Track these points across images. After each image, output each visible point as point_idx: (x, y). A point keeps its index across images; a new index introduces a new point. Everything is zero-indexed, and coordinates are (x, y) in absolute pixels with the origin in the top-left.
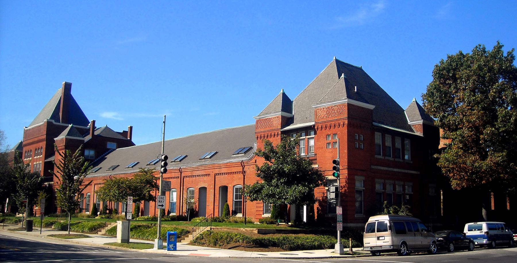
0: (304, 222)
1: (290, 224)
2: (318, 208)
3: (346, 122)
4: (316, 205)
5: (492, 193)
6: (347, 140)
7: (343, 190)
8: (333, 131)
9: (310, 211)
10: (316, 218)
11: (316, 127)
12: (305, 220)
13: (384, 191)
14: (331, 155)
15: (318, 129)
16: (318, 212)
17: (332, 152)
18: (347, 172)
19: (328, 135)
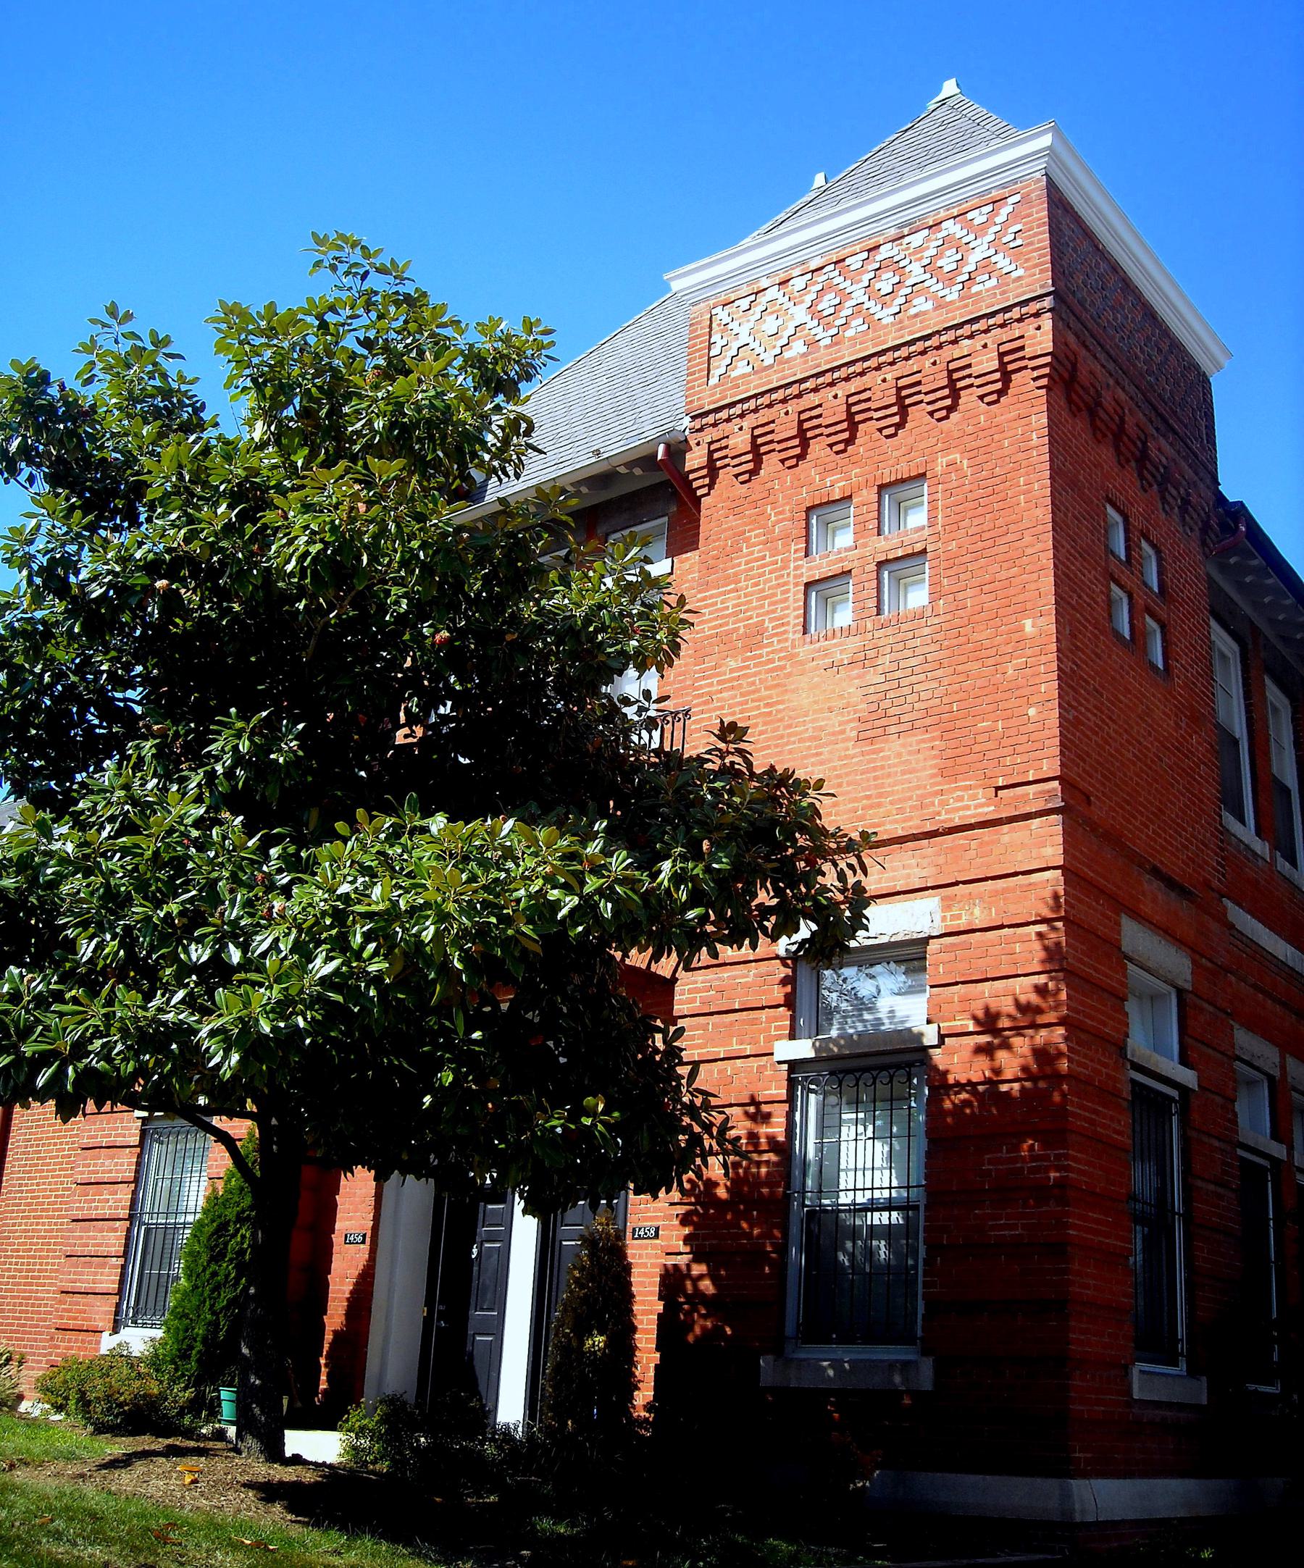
0: (507, 1434)
1: (319, 1446)
2: (672, 1282)
3: (1040, 338)
4: (655, 1234)
5: (691, 1338)
6: (1043, 514)
7: (1011, 1062)
8: (878, 454)
9: (586, 1294)
10: (644, 1395)
11: (695, 459)
12: (511, 1407)
13: (1279, 1151)
14: (853, 692)
15: (712, 470)
16: (669, 1328)
17: (862, 661)
18: (1054, 852)
19: (821, 510)
